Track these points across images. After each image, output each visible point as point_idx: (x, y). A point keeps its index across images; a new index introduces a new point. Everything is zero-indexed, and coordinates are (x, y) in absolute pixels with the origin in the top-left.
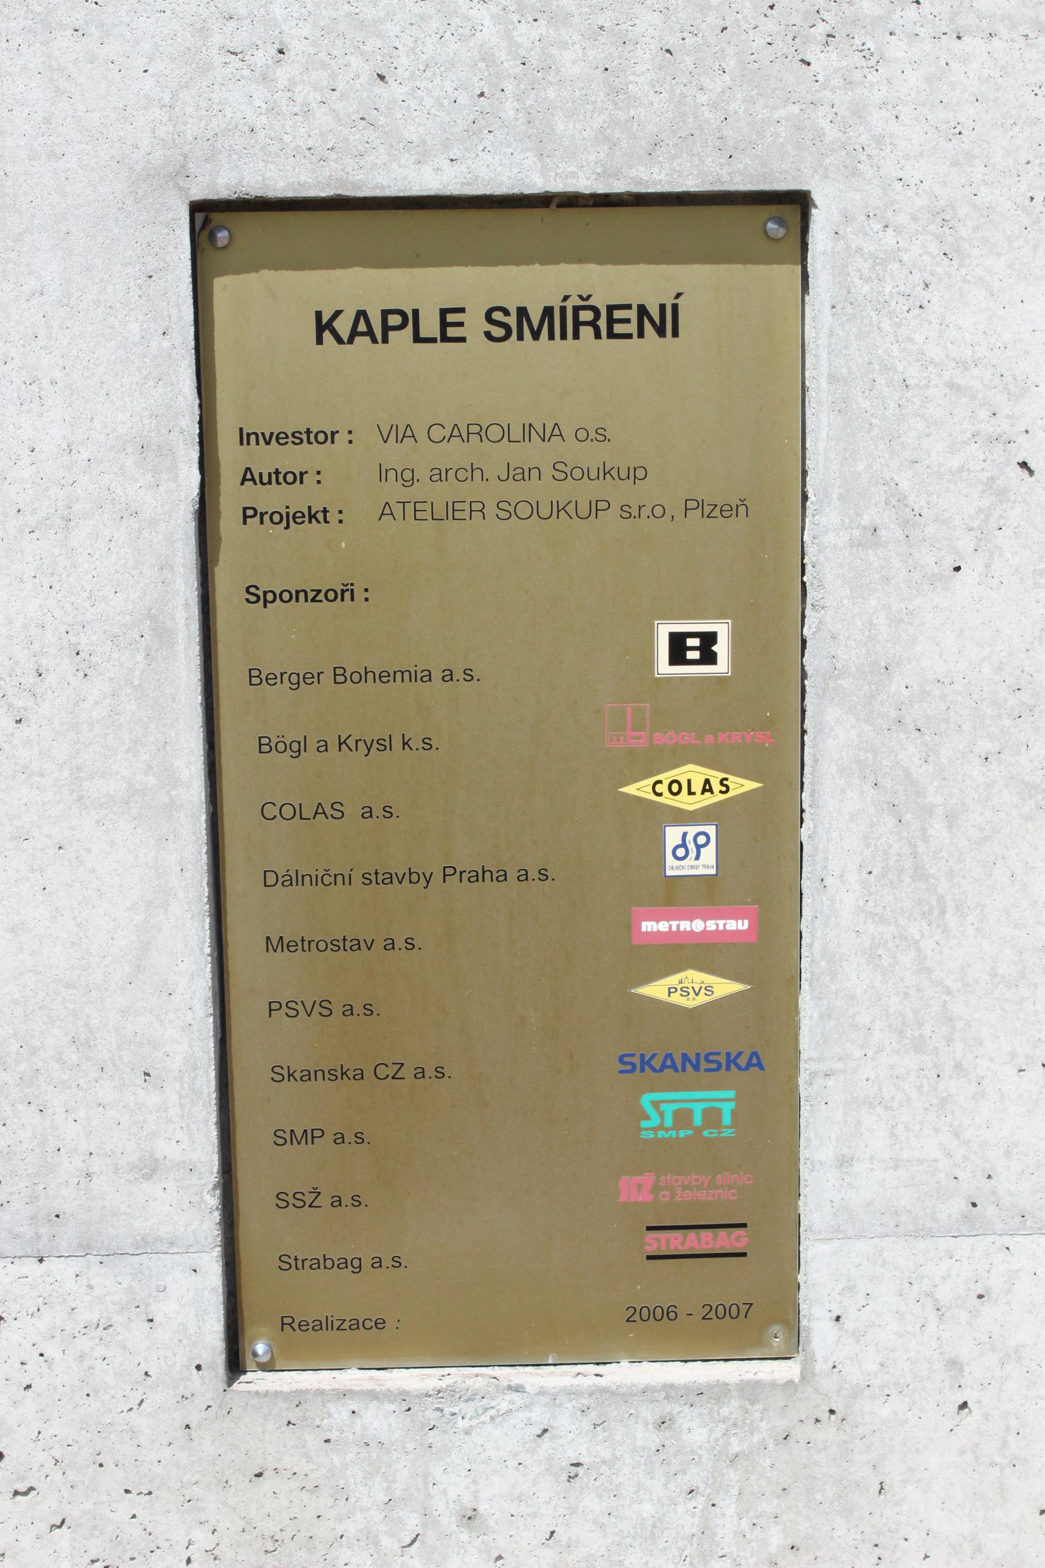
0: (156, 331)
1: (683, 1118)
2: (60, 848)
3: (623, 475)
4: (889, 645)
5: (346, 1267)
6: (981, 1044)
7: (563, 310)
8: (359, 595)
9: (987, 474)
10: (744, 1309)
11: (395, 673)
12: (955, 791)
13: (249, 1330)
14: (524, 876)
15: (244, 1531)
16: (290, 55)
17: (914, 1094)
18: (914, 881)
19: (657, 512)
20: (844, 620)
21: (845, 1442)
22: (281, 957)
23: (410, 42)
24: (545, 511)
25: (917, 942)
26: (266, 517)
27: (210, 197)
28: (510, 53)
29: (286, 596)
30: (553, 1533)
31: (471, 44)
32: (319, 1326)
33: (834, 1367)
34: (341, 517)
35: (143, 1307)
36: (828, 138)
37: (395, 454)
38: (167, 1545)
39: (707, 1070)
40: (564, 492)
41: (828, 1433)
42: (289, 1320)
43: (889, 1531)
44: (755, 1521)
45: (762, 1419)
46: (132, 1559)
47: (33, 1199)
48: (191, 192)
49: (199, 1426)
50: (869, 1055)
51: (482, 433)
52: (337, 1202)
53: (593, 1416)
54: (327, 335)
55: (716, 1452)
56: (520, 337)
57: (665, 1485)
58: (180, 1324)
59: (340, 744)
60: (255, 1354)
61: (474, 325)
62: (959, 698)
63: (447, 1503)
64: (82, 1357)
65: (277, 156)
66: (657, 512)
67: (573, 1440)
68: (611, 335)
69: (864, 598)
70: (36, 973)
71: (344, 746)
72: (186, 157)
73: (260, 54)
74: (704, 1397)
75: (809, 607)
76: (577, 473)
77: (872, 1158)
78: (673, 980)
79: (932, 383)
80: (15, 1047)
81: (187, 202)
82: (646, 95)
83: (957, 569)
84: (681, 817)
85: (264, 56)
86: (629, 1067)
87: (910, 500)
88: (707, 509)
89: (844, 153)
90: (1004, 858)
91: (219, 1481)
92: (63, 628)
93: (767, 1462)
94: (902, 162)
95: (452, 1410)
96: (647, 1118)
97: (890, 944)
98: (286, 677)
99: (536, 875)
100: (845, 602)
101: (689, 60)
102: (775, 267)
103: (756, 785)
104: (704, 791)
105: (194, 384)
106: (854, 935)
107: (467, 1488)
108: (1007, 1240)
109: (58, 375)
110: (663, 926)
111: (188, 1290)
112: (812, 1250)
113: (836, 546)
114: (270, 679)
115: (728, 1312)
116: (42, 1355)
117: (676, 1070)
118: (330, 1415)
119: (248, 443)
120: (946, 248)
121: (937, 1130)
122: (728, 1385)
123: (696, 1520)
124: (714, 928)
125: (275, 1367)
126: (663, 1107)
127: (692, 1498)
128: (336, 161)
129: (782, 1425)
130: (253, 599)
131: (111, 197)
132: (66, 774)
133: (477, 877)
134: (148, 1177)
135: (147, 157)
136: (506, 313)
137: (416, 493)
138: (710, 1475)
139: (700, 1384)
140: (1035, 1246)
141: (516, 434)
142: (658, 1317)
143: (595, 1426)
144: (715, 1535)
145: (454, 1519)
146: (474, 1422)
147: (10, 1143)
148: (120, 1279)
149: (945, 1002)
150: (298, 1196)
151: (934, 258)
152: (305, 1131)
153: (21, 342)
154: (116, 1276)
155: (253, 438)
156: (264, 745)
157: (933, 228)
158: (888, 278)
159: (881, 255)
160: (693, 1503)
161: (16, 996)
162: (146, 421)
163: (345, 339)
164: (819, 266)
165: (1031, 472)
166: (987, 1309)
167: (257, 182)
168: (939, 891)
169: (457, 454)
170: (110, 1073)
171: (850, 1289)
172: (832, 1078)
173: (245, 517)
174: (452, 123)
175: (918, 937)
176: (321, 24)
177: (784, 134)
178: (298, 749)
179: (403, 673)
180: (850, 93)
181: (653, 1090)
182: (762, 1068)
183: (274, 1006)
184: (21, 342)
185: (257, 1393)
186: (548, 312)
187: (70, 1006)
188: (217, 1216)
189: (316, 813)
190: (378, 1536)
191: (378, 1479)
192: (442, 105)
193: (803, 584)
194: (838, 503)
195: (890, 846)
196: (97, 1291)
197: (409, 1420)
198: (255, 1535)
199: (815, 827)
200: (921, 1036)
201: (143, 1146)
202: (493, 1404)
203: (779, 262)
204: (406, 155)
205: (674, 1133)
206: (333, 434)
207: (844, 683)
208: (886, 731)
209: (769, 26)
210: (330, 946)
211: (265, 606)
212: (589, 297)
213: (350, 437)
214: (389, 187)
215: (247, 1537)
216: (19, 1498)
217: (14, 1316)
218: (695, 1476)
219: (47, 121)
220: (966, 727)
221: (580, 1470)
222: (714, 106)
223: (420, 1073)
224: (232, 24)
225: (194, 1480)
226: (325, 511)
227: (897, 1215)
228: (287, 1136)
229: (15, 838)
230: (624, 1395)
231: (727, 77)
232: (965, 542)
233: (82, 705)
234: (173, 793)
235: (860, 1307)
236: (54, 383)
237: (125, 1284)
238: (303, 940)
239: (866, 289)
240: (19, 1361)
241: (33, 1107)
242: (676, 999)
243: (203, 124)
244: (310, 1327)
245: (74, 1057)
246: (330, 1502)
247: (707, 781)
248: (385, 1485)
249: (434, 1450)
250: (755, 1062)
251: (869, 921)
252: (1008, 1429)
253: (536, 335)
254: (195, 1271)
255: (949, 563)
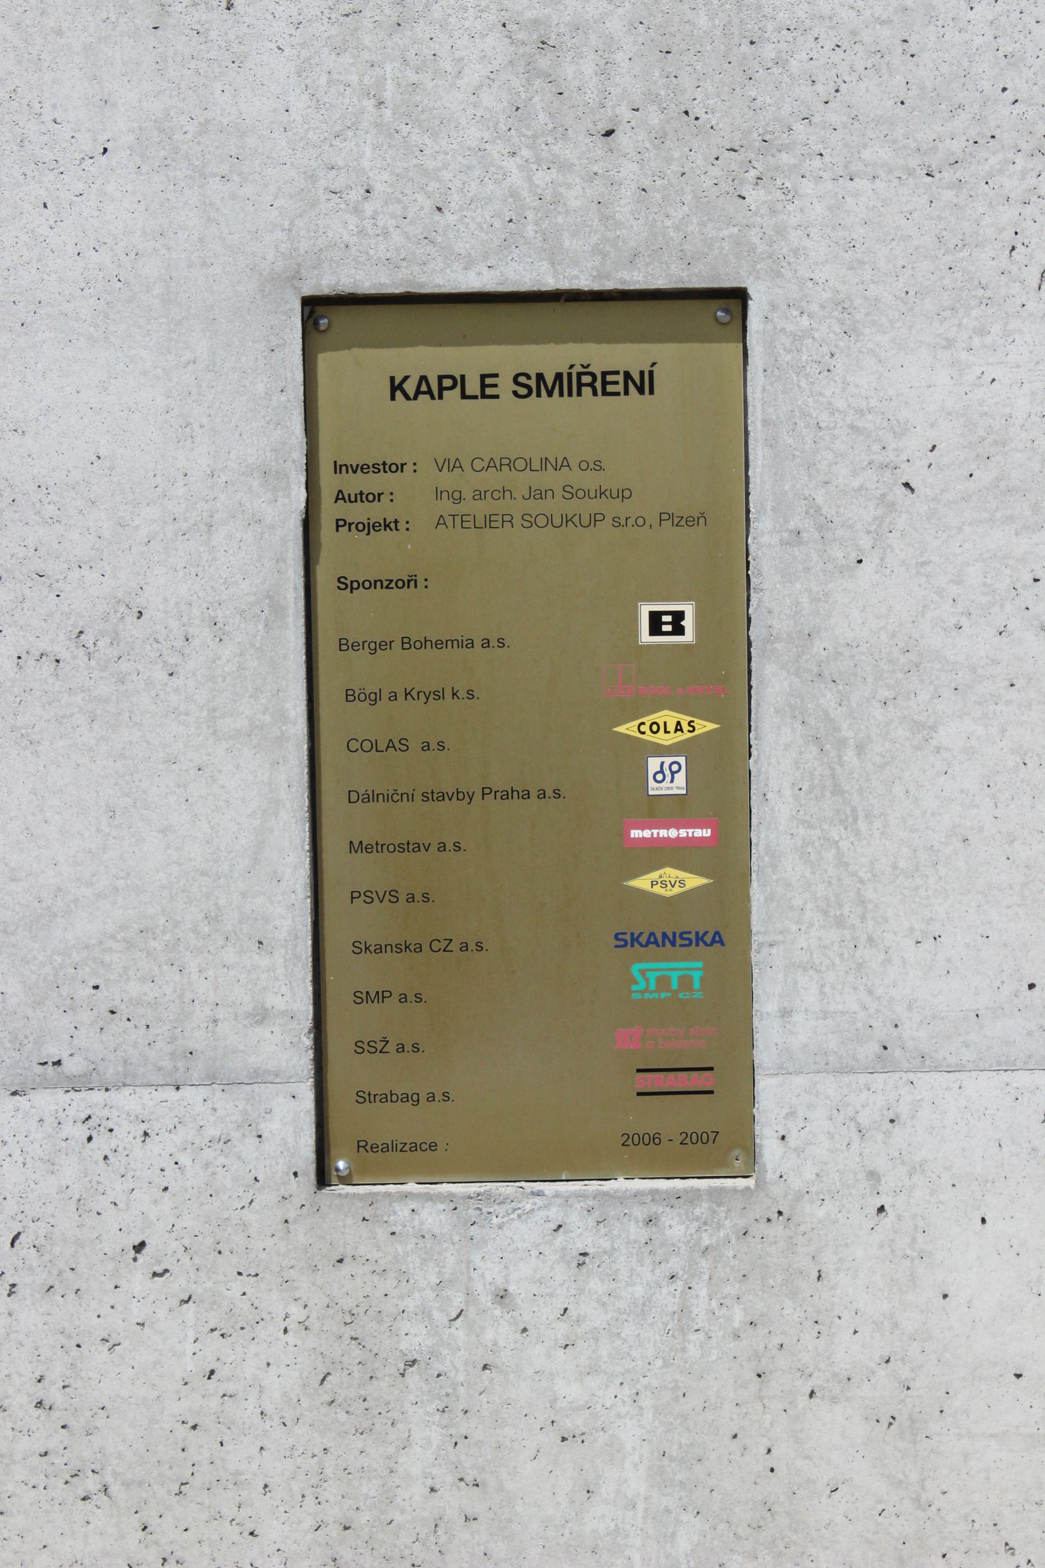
0: (276, 389)
1: (663, 983)
2: (199, 769)
3: (615, 495)
4: (811, 618)
5: (408, 1101)
6: (887, 921)
7: (570, 375)
8: (421, 583)
9: (879, 492)
10: (712, 1136)
11: (447, 641)
12: (862, 727)
13: (334, 1151)
14: (542, 795)
15: (328, 1307)
16: (375, 194)
17: (837, 961)
18: (833, 796)
19: (641, 522)
20: (777, 599)
21: (791, 1238)
22: (361, 856)
23: (459, 184)
24: (557, 521)
25: (837, 842)
26: (353, 527)
27: (317, 293)
28: (530, 191)
29: (367, 584)
30: (566, 1310)
31: (504, 185)
32: (386, 1148)
33: (781, 1177)
34: (407, 526)
35: (254, 1126)
36: (759, 251)
37: (447, 480)
38: (269, 1317)
39: (681, 946)
40: (572, 507)
41: (777, 1229)
42: (363, 1144)
43: (826, 1310)
44: (722, 1301)
45: (726, 1218)
46: (242, 1328)
47: (173, 1040)
48: (303, 290)
49: (295, 1221)
50: (802, 929)
51: (511, 464)
52: (401, 1049)
53: (596, 1214)
54: (398, 394)
55: (691, 1245)
56: (539, 395)
57: (653, 1271)
58: (282, 1139)
59: (406, 695)
60: (337, 1170)
61: (505, 386)
62: (864, 658)
63: (485, 1284)
64: (207, 1165)
65: (365, 265)
66: (641, 522)
67: (581, 1234)
68: (605, 393)
69: (791, 583)
70: (179, 864)
71: (409, 696)
72: (299, 265)
73: (353, 192)
74: (681, 1200)
75: (752, 590)
76: (581, 494)
77: (806, 1010)
78: (654, 875)
79: (838, 425)
80: (162, 920)
81: (300, 297)
82: (628, 221)
83: (860, 561)
84: (660, 750)
85: (355, 195)
86: (622, 943)
87: (824, 511)
88: (676, 520)
89: (770, 261)
90: (900, 778)
91: (310, 1266)
92: (205, 606)
93: (731, 1254)
94: (813, 267)
95: (489, 1210)
96: (637, 983)
97: (816, 844)
98: (366, 645)
99: (552, 794)
100: (778, 586)
101: (658, 196)
102: (724, 345)
103: (716, 726)
104: (676, 730)
105: (303, 428)
106: (789, 837)
107: (500, 1272)
108: (911, 1076)
109: (205, 420)
110: (647, 834)
111: (288, 1112)
112: (763, 1083)
113: (770, 544)
114: (355, 646)
115: (700, 1139)
116: (176, 1163)
117: (658, 946)
118: (395, 1213)
119: (341, 472)
120: (846, 328)
121: (855, 989)
122: (699, 1190)
123: (676, 1300)
124: (685, 835)
125: (352, 1180)
126: (648, 974)
127: (673, 1282)
128: (406, 268)
129: (741, 1223)
130: (343, 586)
131: (246, 294)
132: (205, 714)
133: (507, 795)
134: (260, 1023)
135: (272, 266)
136: (528, 377)
137: (462, 508)
138: (687, 1264)
139: (678, 1190)
140: (933, 1081)
141: (536, 465)
142: (646, 1142)
143: (598, 1222)
144: (691, 1312)
145: (489, 1298)
146: (505, 1219)
147: (156, 995)
148: (237, 1103)
149: (859, 889)
150: (372, 1044)
151: (837, 335)
152: (378, 992)
153: (179, 397)
154: (234, 1101)
155: (344, 468)
156: (350, 696)
157: (836, 313)
158: (804, 349)
159: (799, 333)
160: (674, 1287)
161: (164, 882)
162: (268, 454)
163: (412, 396)
164: (754, 342)
165: (912, 490)
166: (897, 1130)
167: (350, 283)
168: (853, 803)
169: (492, 479)
170: (233, 942)
171: (792, 1114)
172: (775, 947)
173: (338, 526)
174: (489, 241)
175: (837, 839)
176: (397, 172)
177: (727, 248)
178: (374, 698)
179: (452, 641)
180: (774, 219)
181: (640, 961)
182: (723, 944)
183: (356, 895)
184: (179, 397)
185: (340, 1194)
186: (559, 376)
187: (204, 890)
188: (311, 1054)
189: (388, 747)
190: (430, 1311)
191: (432, 1265)
192: (482, 228)
193: (748, 576)
194: (771, 513)
195: (815, 769)
196: (219, 1113)
197: (455, 1216)
198: (336, 1310)
199: (759, 755)
200: (842, 915)
201: (257, 998)
202: (520, 1206)
203: (727, 341)
204: (457, 264)
205: (656, 995)
206: (402, 465)
207: (777, 646)
208: (810, 683)
209: (715, 172)
210: (397, 848)
211: (352, 592)
212: (588, 365)
213: (415, 468)
214: (444, 286)
215: (330, 1311)
216: (156, 1279)
217: (156, 1131)
218: (675, 1264)
219: (201, 240)
220: (870, 679)
221: (587, 1259)
222: (677, 228)
223: (465, 947)
224: (334, 172)
225: (290, 1265)
226: (396, 522)
227: (827, 1056)
228: (364, 996)
229: (167, 762)
230: (620, 1199)
231: (686, 208)
232: (865, 542)
233: (218, 662)
234: (284, 728)
235: (800, 1129)
236: (202, 426)
237: (241, 1107)
238: (377, 844)
239: (788, 357)
240: (160, 1167)
241: (175, 968)
242: (657, 890)
243: (312, 242)
244: (380, 1149)
245: (206, 929)
246: (395, 1284)
247: (679, 723)
248: (437, 1269)
249: (475, 1241)
250: (718, 939)
251: (801, 826)
252: (916, 1227)
253: (550, 394)
254: (294, 1097)
255: (854, 556)
